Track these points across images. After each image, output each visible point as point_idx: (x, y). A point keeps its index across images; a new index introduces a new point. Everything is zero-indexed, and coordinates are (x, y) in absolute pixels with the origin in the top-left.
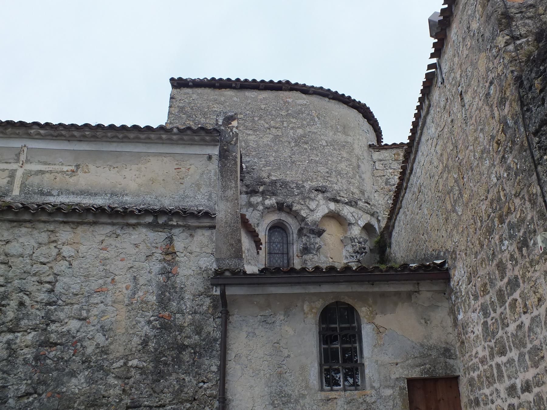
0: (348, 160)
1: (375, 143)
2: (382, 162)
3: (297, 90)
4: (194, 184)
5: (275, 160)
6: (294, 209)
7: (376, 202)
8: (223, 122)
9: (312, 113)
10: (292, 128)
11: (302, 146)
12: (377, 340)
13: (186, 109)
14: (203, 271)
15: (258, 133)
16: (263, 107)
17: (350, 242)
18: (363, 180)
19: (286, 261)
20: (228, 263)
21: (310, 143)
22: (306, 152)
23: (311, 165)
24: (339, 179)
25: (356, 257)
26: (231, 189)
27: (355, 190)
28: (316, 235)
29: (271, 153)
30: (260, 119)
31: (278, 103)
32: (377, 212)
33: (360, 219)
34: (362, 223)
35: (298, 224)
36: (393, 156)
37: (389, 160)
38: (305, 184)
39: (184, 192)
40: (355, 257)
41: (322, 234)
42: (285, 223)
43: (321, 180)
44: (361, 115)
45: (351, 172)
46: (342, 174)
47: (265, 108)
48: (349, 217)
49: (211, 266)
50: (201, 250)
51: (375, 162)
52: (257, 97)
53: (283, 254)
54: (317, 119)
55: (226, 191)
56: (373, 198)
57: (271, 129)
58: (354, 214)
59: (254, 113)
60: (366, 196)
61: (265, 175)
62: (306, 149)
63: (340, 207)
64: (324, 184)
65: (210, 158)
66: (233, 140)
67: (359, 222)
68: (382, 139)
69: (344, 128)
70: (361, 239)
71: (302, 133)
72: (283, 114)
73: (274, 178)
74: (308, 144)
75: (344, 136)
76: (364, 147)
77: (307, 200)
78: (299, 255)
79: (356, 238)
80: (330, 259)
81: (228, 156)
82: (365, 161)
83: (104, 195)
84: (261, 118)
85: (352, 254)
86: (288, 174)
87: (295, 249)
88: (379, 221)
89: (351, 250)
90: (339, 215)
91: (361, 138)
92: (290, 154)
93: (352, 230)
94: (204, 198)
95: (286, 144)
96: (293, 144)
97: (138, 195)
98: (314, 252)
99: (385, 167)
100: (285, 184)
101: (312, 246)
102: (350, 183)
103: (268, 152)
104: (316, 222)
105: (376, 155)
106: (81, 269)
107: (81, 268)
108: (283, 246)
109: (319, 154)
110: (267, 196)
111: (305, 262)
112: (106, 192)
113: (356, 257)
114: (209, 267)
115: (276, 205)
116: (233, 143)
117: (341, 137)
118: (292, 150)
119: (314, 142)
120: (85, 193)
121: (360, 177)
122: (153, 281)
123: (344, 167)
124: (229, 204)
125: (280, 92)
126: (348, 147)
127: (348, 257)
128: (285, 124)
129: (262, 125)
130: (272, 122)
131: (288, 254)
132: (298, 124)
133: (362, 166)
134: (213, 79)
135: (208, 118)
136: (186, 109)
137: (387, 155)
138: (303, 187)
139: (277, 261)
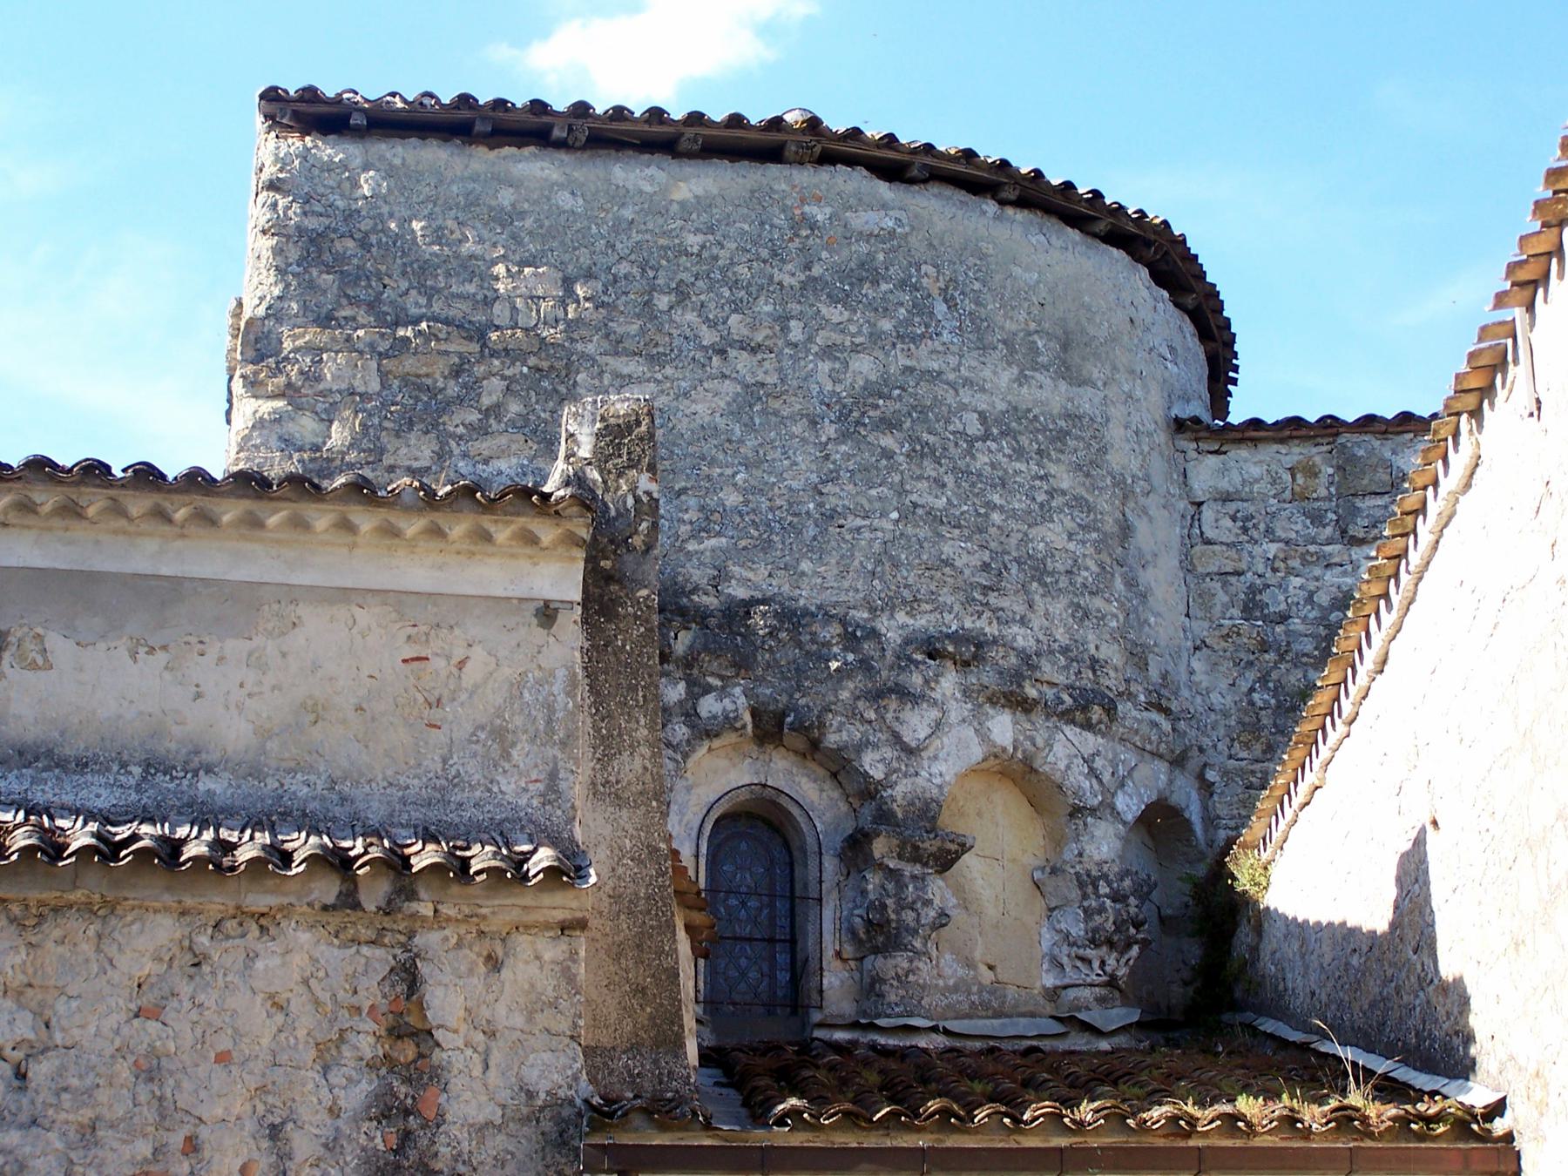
0: (1079, 503)
1: (1198, 408)
2: (1232, 507)
3: (851, 161)
4: (483, 728)
5: (746, 502)
6: (832, 739)
7: (1199, 699)
8: (596, 450)
9: (920, 277)
10: (828, 352)
11: (871, 438)
12: (902, 906)
13: (338, 246)
14: (542, 1109)
15: (669, 371)
16: (693, 241)
17: (1075, 894)
18: (1144, 596)
19: (783, 977)
20: (627, 1065)
21: (908, 424)
22: (891, 469)
23: (910, 530)
24: (1037, 598)
25: (1103, 963)
26: (633, 748)
27: (1111, 653)
28: (925, 865)
29: (729, 471)
30: (679, 303)
31: (762, 224)
32: (1201, 750)
33: (1122, 785)
34: (1129, 805)
35: (844, 807)
36: (1287, 477)
37: (1264, 498)
38: (883, 624)
39: (445, 761)
40: (1096, 964)
41: (954, 861)
42: (784, 801)
43: (957, 607)
44: (1145, 272)
45: (1090, 563)
46: (1052, 574)
47: (703, 247)
48: (1077, 778)
49: (570, 1087)
50: (530, 1019)
51: (1200, 504)
52: (664, 190)
53: (771, 940)
54: (940, 308)
55: (611, 757)
56: (1184, 677)
57: (732, 353)
58: (1099, 763)
59: (651, 274)
60: (1154, 673)
61: (698, 575)
62: (888, 454)
63: (1040, 729)
64: (968, 624)
65: (547, 614)
66: (636, 532)
67: (1121, 802)
68: (1236, 369)
69: (1065, 347)
70: (1127, 883)
71: (873, 378)
72: (788, 280)
73: (741, 593)
74: (900, 430)
75: (1063, 386)
76: (1150, 434)
77: (893, 703)
78: (848, 951)
79: (1105, 877)
80: (983, 969)
81: (616, 602)
82: (1153, 503)
83: (115, 768)
84: (682, 294)
85: (1081, 952)
86: (803, 574)
87: (828, 926)
88: (1206, 788)
89: (1078, 930)
90: (1033, 770)
91: (1139, 393)
92: (814, 478)
93: (1086, 838)
94: (525, 790)
95: (797, 429)
96: (830, 430)
97: (256, 773)
98: (918, 944)
99: (1245, 530)
100: (792, 618)
101: (909, 916)
102: (1086, 615)
103: (713, 462)
104: (927, 804)
105: (1207, 473)
106: (65, 1096)
107: (65, 1089)
108: (772, 906)
109: (949, 480)
110: (710, 680)
111: (872, 985)
112: (125, 757)
113: (1103, 963)
114: (561, 1093)
115: (747, 718)
116: (637, 541)
117: (1048, 395)
118: (827, 457)
119: (926, 421)
120: (37, 759)
121: (1131, 583)
122: (348, 1149)
123: (1060, 541)
124: (625, 813)
125: (774, 169)
126: (1078, 438)
127: (1065, 960)
128: (796, 332)
129: (688, 333)
130: (734, 319)
131: (793, 941)
132: (853, 329)
133: (1141, 527)
134: (465, 100)
135: (438, 291)
136: (338, 246)
137: (1256, 471)
138: (874, 634)
139: (743, 974)
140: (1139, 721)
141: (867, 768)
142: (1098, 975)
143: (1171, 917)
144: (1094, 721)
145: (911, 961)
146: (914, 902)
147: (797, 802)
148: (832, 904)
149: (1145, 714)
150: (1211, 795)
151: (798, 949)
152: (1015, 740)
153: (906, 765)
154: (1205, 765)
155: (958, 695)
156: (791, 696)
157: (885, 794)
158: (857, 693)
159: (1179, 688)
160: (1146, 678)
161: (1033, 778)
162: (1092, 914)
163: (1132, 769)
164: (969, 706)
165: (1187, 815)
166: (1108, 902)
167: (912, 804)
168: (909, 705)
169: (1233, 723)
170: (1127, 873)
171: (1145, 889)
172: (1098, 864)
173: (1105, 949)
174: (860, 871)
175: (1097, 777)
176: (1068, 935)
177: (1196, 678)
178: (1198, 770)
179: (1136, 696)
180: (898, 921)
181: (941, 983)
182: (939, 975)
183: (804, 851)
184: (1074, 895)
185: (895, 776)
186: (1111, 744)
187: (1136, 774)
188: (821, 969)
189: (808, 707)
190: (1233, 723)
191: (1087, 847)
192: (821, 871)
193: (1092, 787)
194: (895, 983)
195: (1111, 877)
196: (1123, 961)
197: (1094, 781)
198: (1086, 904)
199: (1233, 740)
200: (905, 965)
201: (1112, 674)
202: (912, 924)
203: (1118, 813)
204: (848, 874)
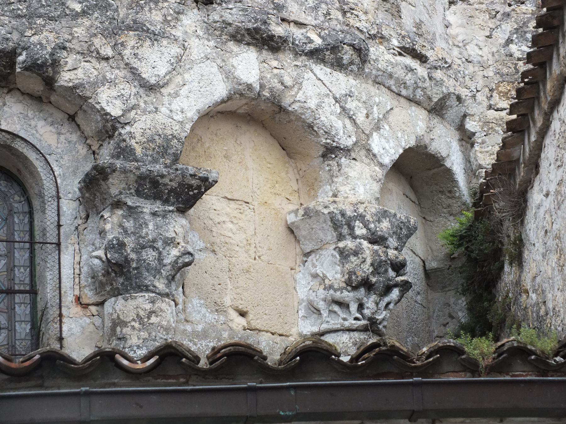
7: (456, 52)
17: (331, 235)
25: (361, 307)
28: (166, 202)
33: (377, 128)
40: (354, 307)
42: (19, 146)
56: (439, 29)
58: (351, 105)
60: (408, 21)
77: (131, 39)
79: (361, 217)
80: (234, 315)
87: (67, 272)
93: (340, 179)
98: (161, 285)
101: (150, 255)
104: (168, 141)
113: (361, 307)
131: (33, 292)
140: (394, 65)
141: (104, 105)
142: (356, 319)
143: (436, 270)
144: (345, 62)
145: (153, 302)
146: (154, 241)
147: (34, 146)
148: (71, 248)
149: (399, 58)
150: (472, 145)
151: (39, 299)
152: (261, 78)
153: (145, 102)
154: (465, 116)
155: (200, 33)
156: (22, 35)
157: (123, 131)
158: (93, 31)
159: (434, 38)
160: (400, 25)
161: (283, 115)
162: (348, 256)
163: (388, 112)
164: (212, 43)
165: (448, 164)
166: (365, 244)
167: (152, 140)
168: (148, 43)
169: (491, 74)
170: (385, 214)
171: (404, 232)
172: (355, 205)
173: (362, 290)
174: (98, 213)
175: (350, 118)
176: (324, 278)
177: (452, 31)
178: (457, 121)
179: (388, 40)
180: (139, 260)
181: (189, 328)
182: (187, 321)
183: (41, 196)
184: (329, 238)
185: (133, 113)
186: (364, 85)
187: (391, 118)
188: (61, 315)
189: (40, 44)
190: (491, 74)
191: (341, 188)
192: (59, 215)
193: (345, 127)
194: (137, 325)
195: (368, 217)
196: (383, 304)
197: (347, 121)
198: (341, 245)
199: (491, 90)
200: (148, 306)
201: (363, 17)
202: (154, 264)
203: (374, 155)
204: (87, 217)
